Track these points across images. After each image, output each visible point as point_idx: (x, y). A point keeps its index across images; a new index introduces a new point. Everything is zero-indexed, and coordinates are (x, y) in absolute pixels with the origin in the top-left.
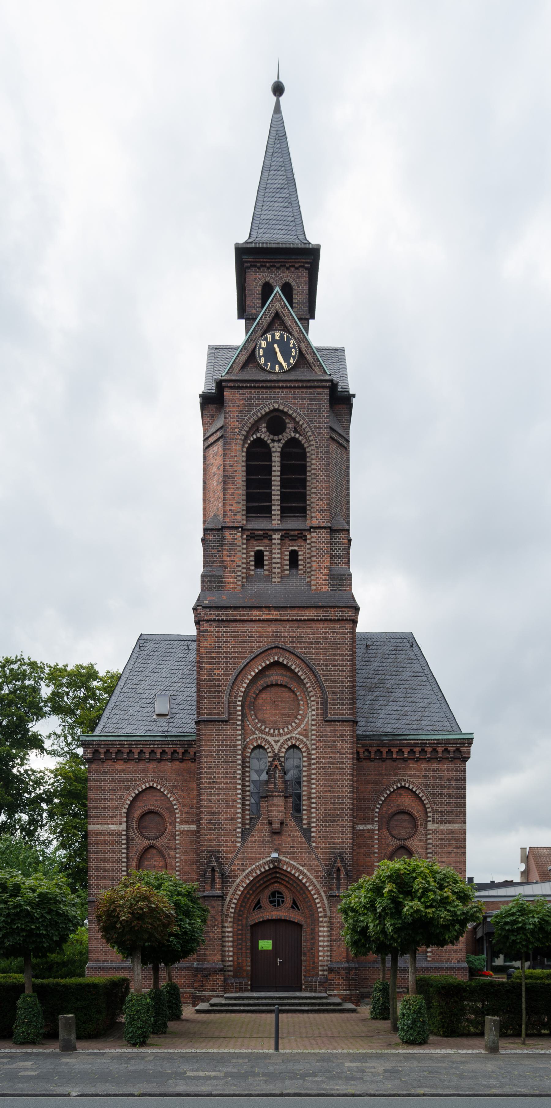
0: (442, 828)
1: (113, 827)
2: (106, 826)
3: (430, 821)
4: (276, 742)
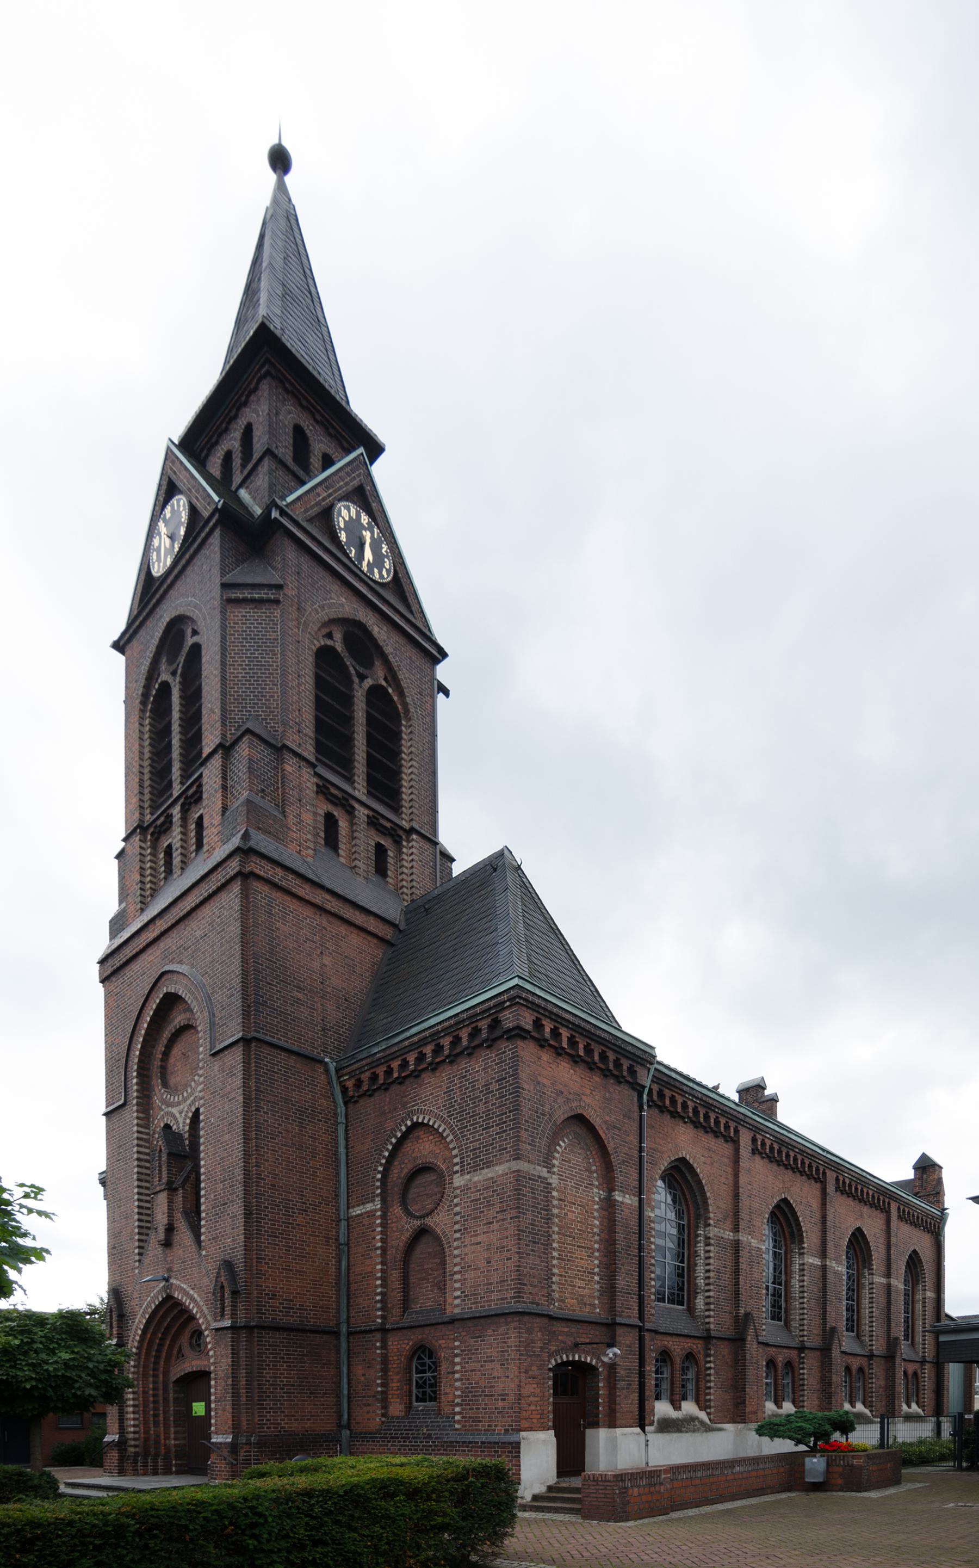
0: (476, 1179)
3: (457, 1172)
4: (180, 1113)
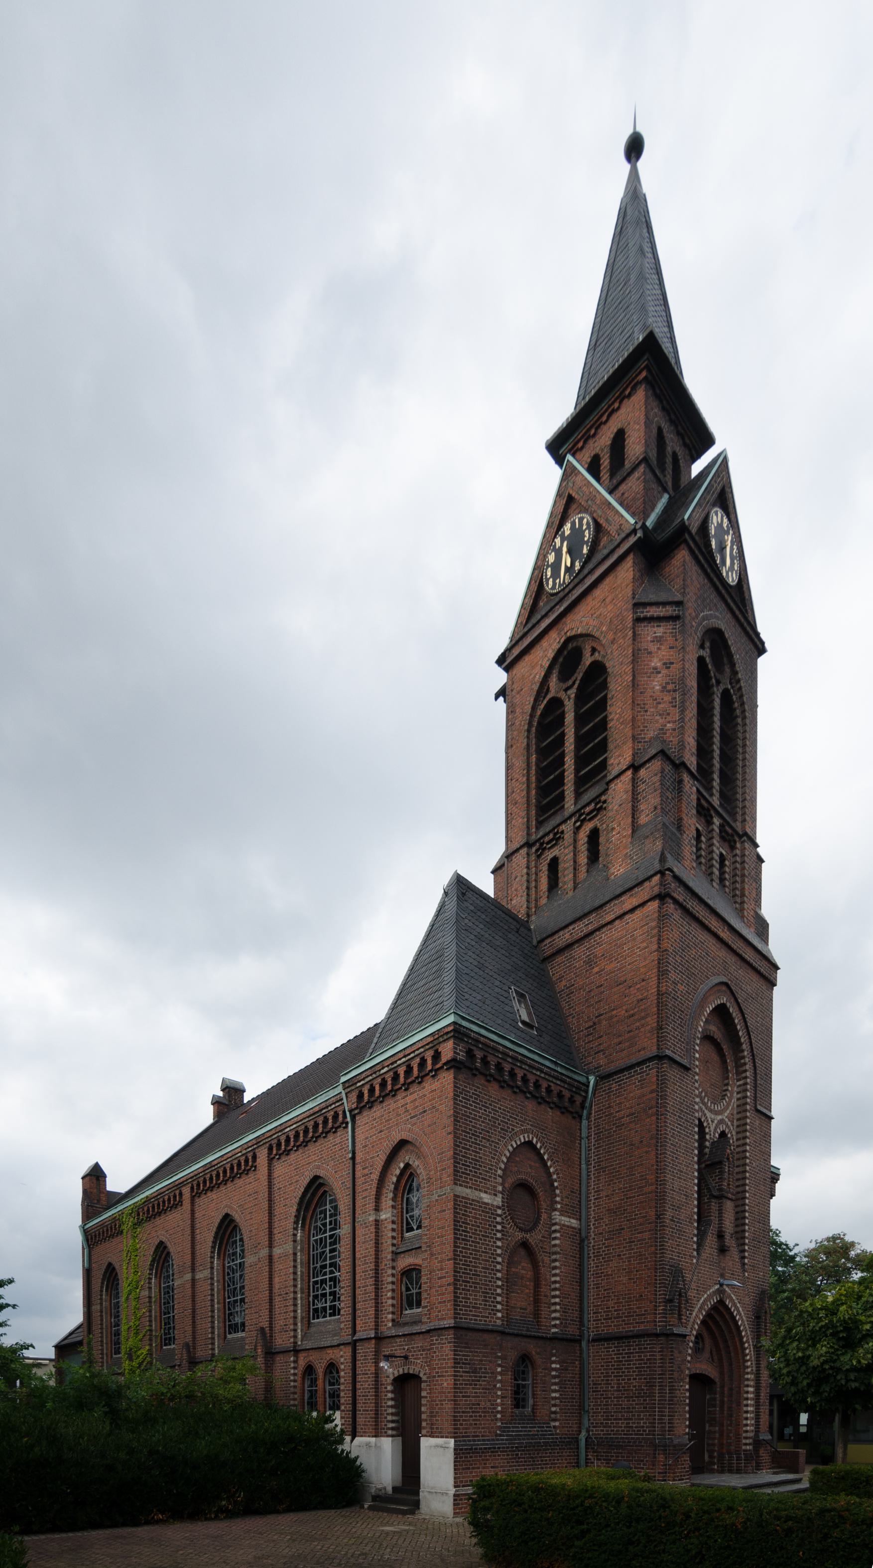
1: (486, 1198)
2: (477, 1193)
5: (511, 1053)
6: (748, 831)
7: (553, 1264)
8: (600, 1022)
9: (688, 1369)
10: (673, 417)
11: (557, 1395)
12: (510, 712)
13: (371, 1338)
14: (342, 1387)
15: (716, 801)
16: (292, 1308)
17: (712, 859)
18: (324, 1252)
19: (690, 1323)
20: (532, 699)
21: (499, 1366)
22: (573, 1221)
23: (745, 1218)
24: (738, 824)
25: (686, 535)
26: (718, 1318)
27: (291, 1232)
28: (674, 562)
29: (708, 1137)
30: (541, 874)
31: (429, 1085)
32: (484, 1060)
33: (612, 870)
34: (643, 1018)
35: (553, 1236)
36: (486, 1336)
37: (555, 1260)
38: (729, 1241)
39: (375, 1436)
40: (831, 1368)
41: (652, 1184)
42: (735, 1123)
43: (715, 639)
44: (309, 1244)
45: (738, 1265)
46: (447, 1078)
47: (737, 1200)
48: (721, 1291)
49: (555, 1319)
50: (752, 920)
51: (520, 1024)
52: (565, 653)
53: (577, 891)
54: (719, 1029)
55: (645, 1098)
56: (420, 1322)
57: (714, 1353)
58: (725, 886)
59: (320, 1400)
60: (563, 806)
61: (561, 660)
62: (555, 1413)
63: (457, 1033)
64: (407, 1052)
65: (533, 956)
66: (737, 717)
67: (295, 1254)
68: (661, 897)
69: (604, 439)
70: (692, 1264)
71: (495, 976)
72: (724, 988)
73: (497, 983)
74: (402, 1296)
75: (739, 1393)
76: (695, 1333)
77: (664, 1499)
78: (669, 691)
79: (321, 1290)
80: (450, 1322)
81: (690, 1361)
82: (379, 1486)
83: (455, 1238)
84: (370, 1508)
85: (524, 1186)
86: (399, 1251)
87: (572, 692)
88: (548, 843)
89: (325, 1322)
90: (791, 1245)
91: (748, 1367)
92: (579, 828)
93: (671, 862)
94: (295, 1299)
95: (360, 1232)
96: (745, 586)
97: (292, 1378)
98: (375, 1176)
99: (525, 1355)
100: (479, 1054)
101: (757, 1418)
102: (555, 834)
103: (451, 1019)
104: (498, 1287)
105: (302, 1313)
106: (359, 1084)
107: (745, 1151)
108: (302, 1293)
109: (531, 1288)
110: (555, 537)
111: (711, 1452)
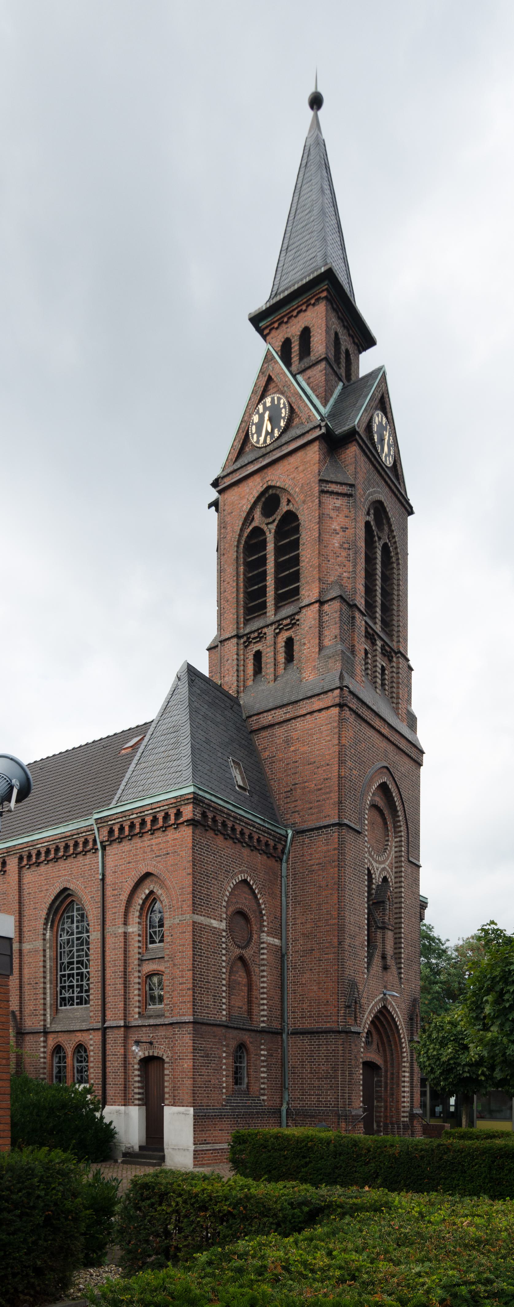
1: (215, 923)
2: (208, 920)
5: (233, 814)
6: (402, 650)
7: (262, 974)
8: (295, 789)
9: (362, 1058)
10: (346, 324)
11: (265, 1075)
12: (222, 526)
13: (120, 1027)
14: (92, 1065)
15: (378, 628)
16: (42, 996)
17: (376, 671)
18: (71, 951)
19: (363, 1023)
20: (241, 523)
21: (224, 1052)
22: (276, 940)
23: (401, 943)
24: (395, 643)
25: (357, 436)
26: (382, 1019)
27: (41, 931)
28: (348, 452)
29: (374, 881)
30: (247, 661)
31: (171, 834)
32: (214, 820)
33: (304, 675)
34: (327, 793)
35: (262, 951)
36: (215, 1029)
37: (263, 971)
38: (390, 962)
39: (124, 1105)
40: (455, 1063)
41: (335, 919)
42: (394, 870)
43: (379, 509)
44: (57, 943)
45: (397, 979)
46: (187, 832)
47: (396, 928)
48: (384, 999)
49: (263, 1016)
50: (405, 716)
51: (237, 788)
52: (267, 495)
53: (276, 682)
54: (381, 799)
55: (329, 854)
56: (163, 1015)
57: (380, 1045)
58: (385, 690)
59: (69, 1075)
60: (266, 613)
61: (263, 499)
62: (263, 1089)
63: (196, 800)
64: (154, 806)
65: (244, 729)
66: (393, 563)
67: (44, 950)
68: (341, 706)
69: (293, 330)
70: (364, 978)
71: (218, 748)
72: (385, 770)
73: (220, 755)
74: (146, 994)
75: (398, 1077)
76: (366, 1030)
77: (355, 1141)
78: (345, 549)
79: (70, 983)
80: (190, 1018)
81: (364, 1052)
82: (128, 1145)
83: (194, 954)
84: (123, 1162)
85: (241, 913)
86: (144, 958)
87: (273, 527)
88: (254, 639)
89: (73, 1009)
90: (443, 940)
91: (404, 1057)
92: (277, 634)
93: (348, 681)
94: (45, 988)
95: (109, 941)
96: (398, 466)
97: (42, 1055)
98: (124, 897)
99: (242, 1044)
100: (210, 815)
101: (412, 1097)
102: (259, 634)
103: (191, 789)
104: (223, 991)
105: (50, 1000)
106: (110, 823)
107: (401, 892)
108: (51, 983)
109: (246, 991)
110: (258, 404)
111: (378, 1123)
